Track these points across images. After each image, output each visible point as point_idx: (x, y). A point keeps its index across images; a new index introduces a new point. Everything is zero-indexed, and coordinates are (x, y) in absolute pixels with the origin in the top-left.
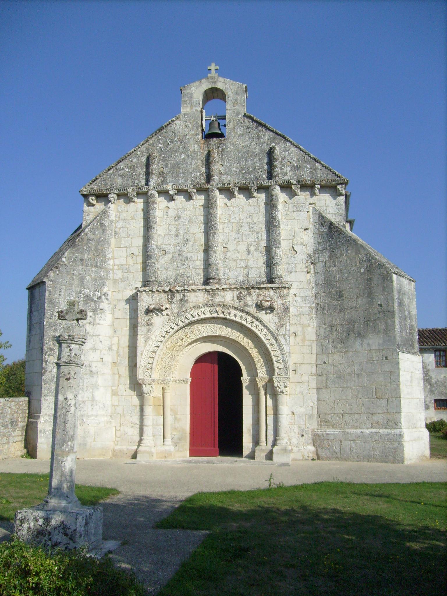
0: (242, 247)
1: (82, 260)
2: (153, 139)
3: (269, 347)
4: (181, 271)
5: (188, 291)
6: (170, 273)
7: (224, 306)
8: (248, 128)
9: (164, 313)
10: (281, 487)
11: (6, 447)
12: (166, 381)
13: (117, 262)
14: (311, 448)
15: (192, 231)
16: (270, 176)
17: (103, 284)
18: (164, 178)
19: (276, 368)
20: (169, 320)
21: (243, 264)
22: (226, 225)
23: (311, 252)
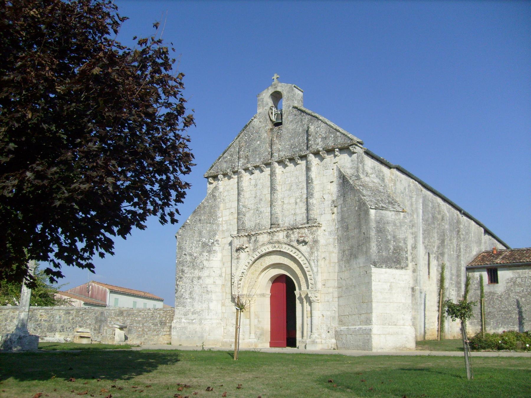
0: (293, 200)
1: (200, 220)
2: (242, 134)
4: (258, 221)
5: (259, 234)
6: (252, 223)
7: (279, 242)
8: (296, 115)
10: (210, 351)
11: (156, 337)
13: (224, 219)
14: (334, 341)
15: (264, 193)
16: (308, 148)
17: (215, 234)
18: (248, 159)
20: (249, 254)
21: (293, 212)
22: (283, 186)
23: (335, 198)
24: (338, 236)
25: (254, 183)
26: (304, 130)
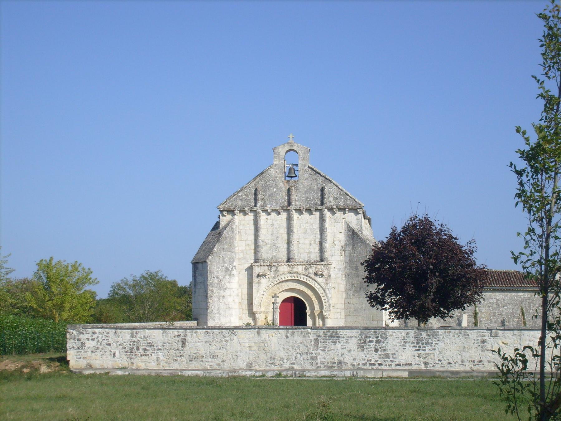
0: (307, 242)
1: (223, 249)
4: (275, 254)
6: (269, 255)
7: (298, 273)
13: (240, 248)
17: (234, 261)
18: (265, 202)
23: (343, 245)
24: (346, 273)
25: (272, 225)
26: (318, 188)
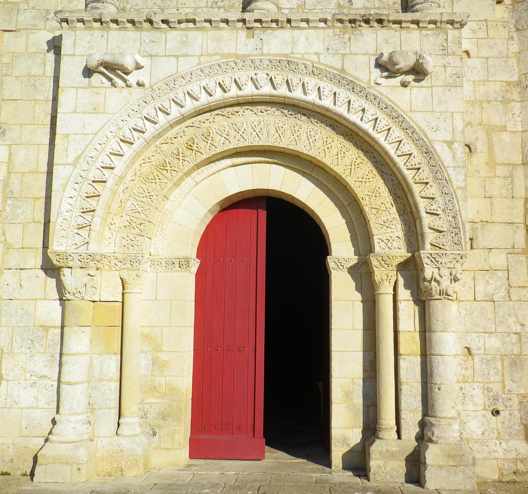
3: (409, 175)
9: (132, 79)
12: (134, 261)
19: (427, 230)
